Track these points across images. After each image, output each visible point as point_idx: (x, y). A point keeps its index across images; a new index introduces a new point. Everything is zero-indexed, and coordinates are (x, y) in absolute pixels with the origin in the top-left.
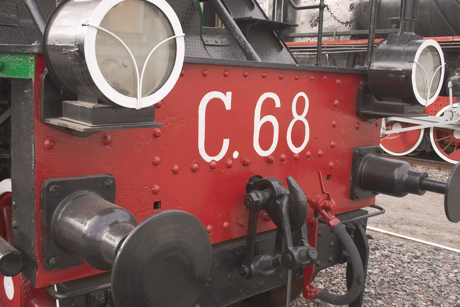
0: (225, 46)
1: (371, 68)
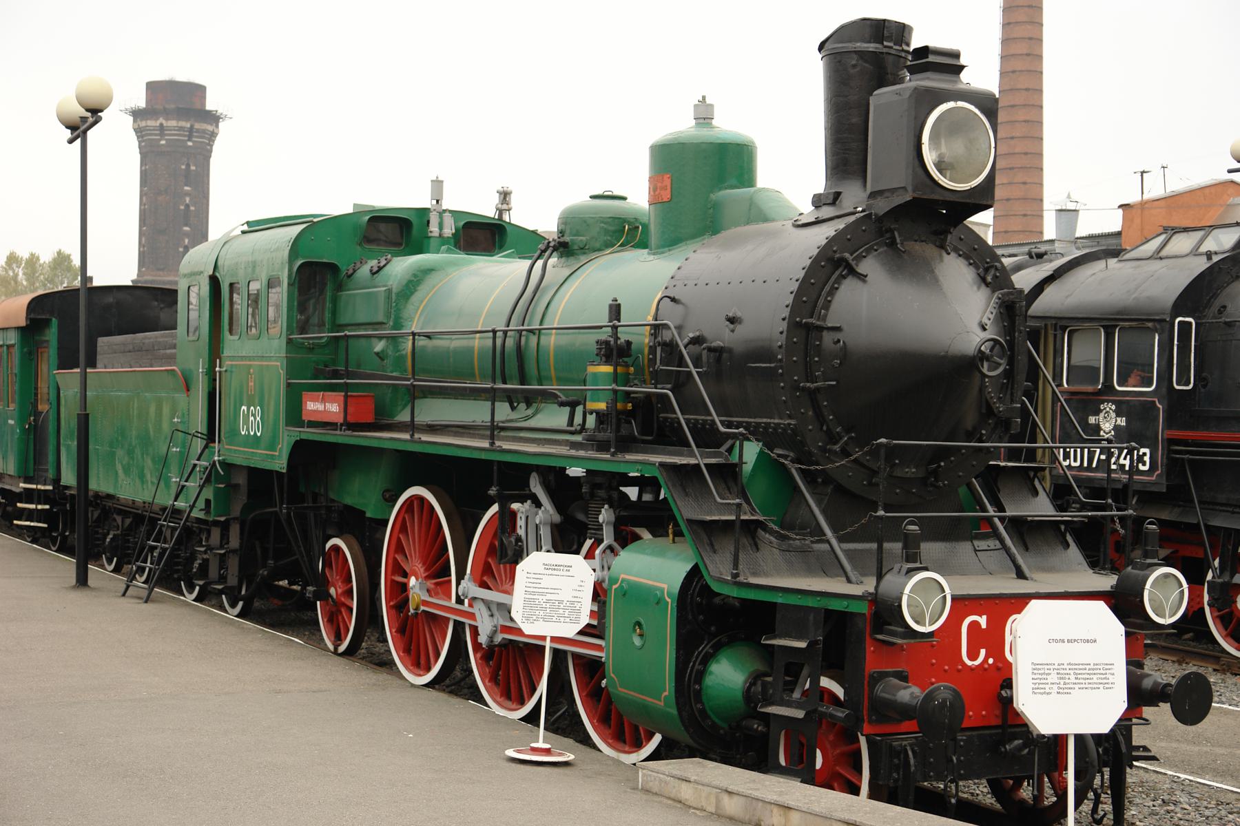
0: (998, 549)
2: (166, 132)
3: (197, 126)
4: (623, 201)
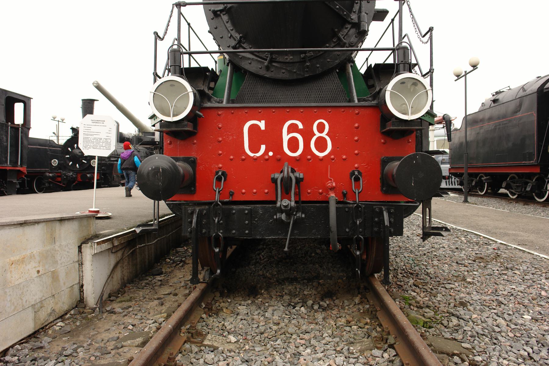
4: (431, 118)
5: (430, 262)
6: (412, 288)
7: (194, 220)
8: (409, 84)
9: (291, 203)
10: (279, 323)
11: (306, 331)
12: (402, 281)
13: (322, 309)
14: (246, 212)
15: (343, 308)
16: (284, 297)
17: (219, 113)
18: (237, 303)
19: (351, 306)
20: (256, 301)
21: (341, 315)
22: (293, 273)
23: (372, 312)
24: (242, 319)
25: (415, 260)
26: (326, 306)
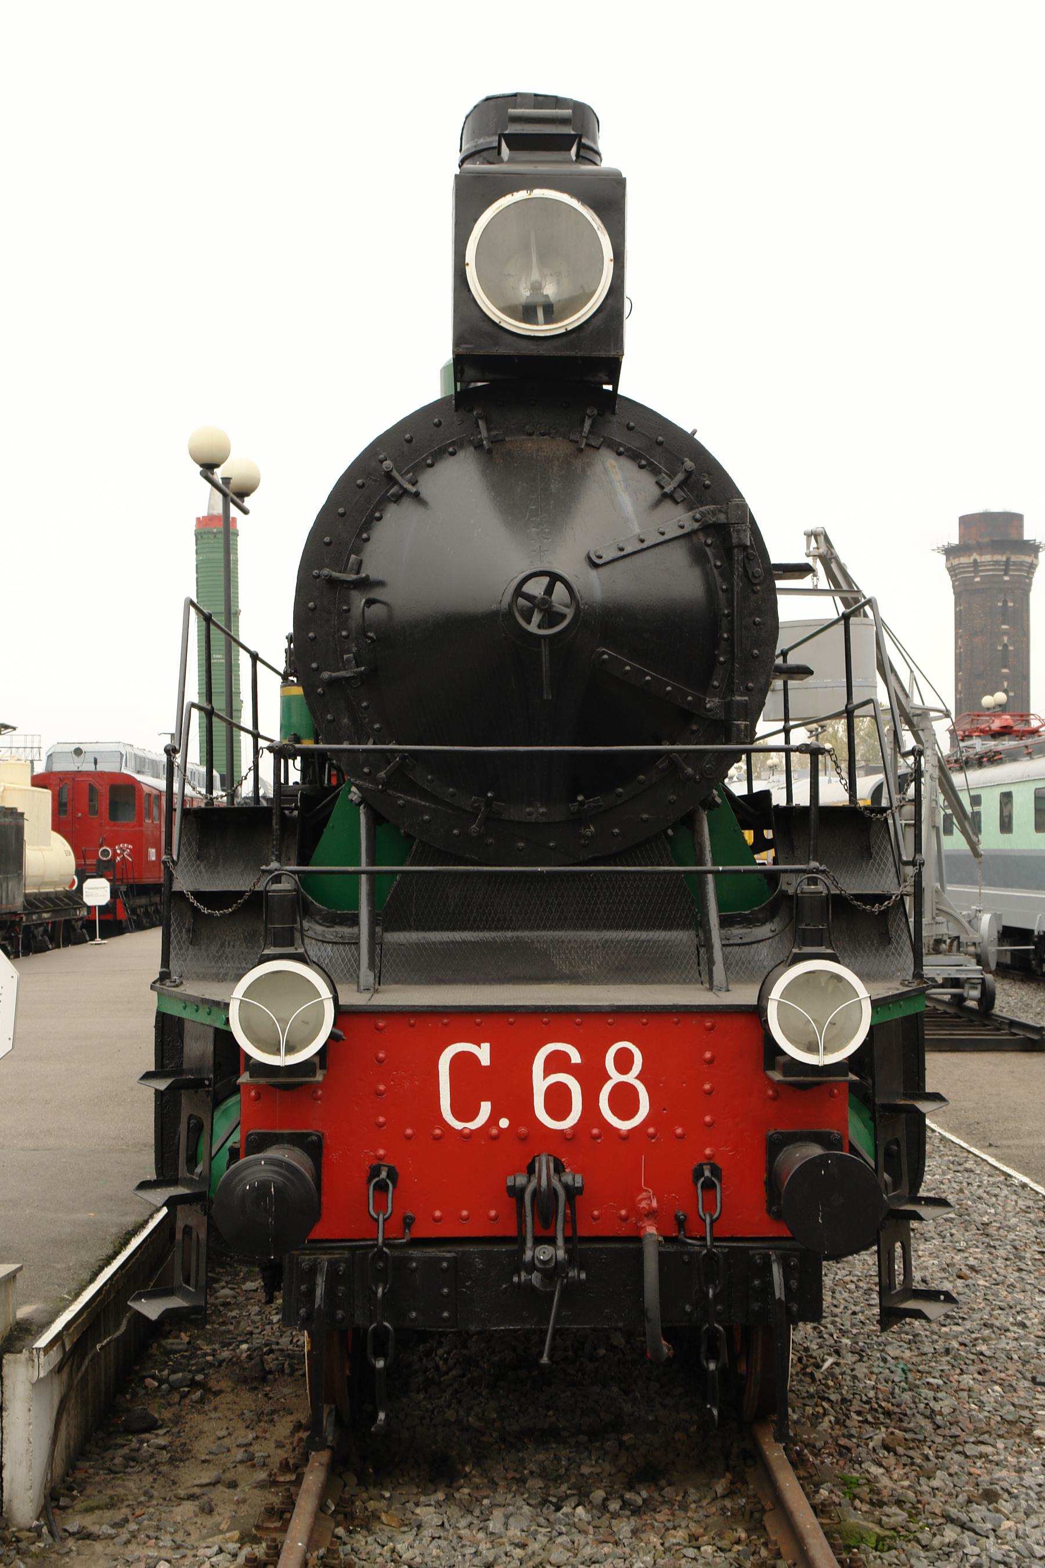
1: (188, 806)
2: (980, 568)
3: (1014, 558)
5: (951, 1379)
6: (876, 1456)
7: (319, 1291)
8: (823, 980)
9: (558, 1252)
10: (526, 1545)
11: (593, 1559)
12: (853, 1436)
13: (631, 1510)
14: (445, 1264)
15: (684, 1507)
16: (530, 1483)
17: (380, 1024)
18: (408, 1502)
19: (704, 1503)
20: (457, 1495)
21: (676, 1524)
22: (546, 1416)
23: (752, 1513)
24: (433, 1538)
25: (910, 1370)
26: (640, 1502)
